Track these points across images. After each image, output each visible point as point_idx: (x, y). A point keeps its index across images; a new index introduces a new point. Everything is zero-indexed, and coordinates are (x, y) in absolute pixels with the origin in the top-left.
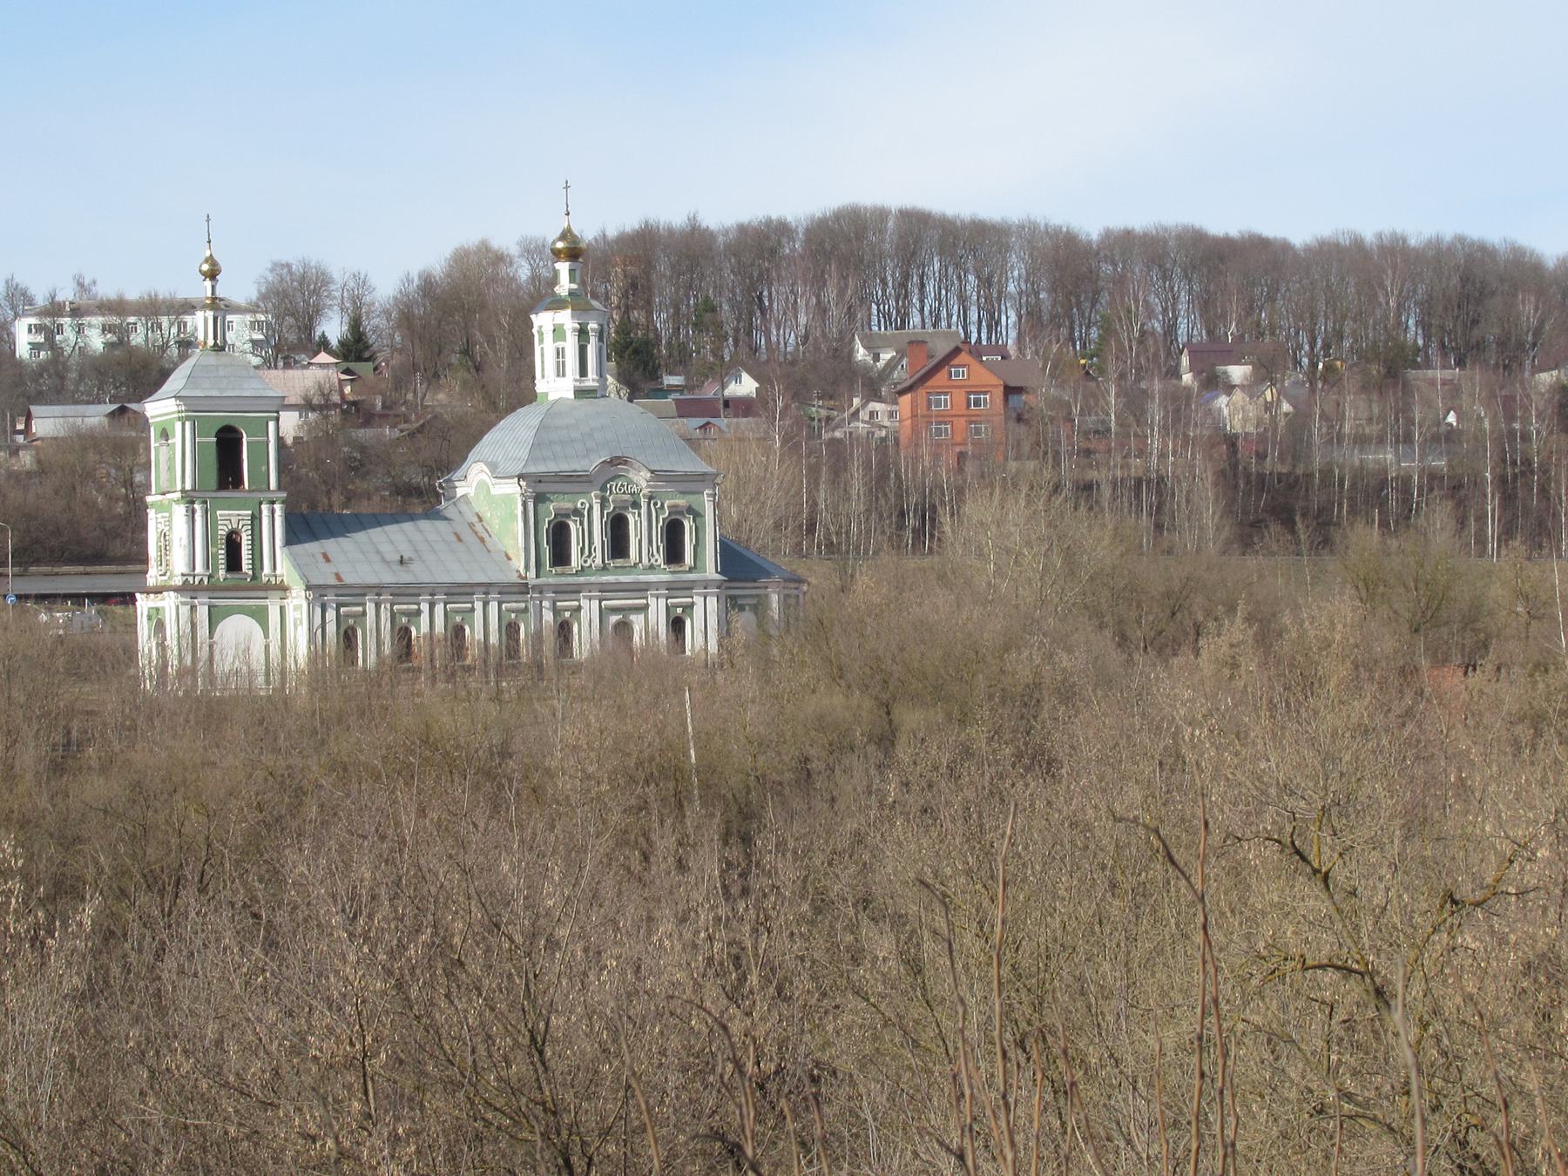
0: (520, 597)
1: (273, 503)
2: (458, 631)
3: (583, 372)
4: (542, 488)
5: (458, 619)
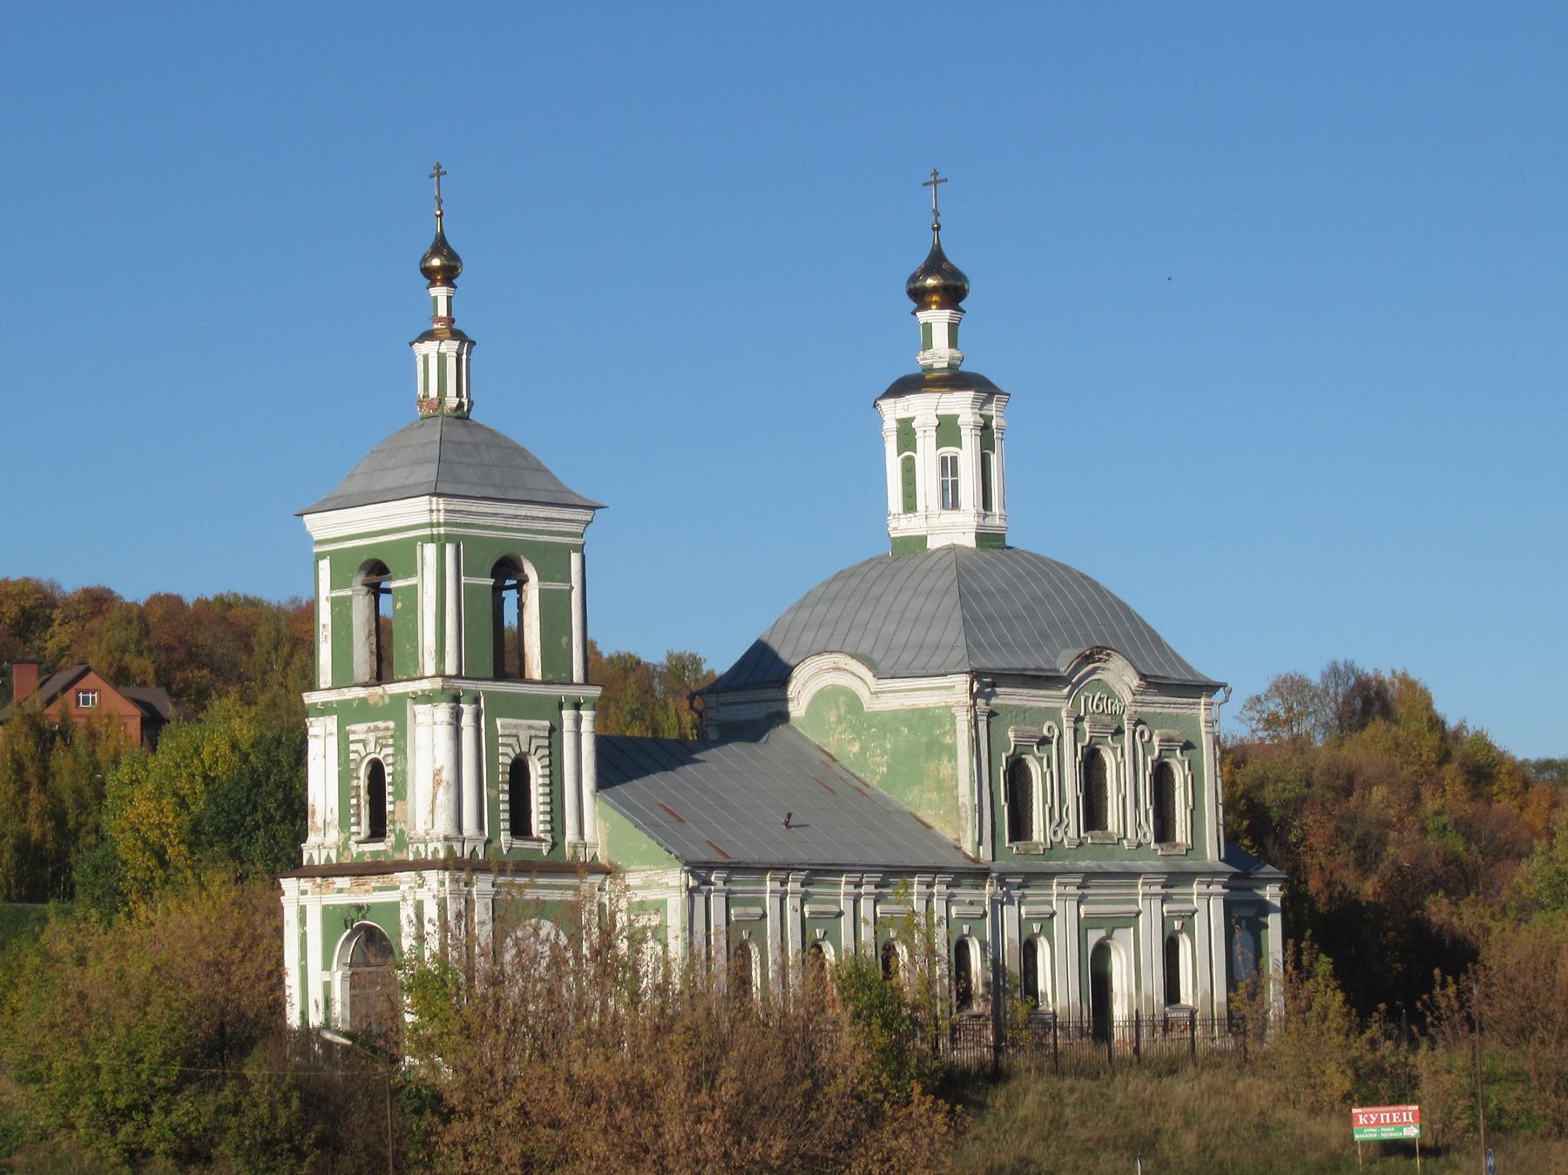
1: (577, 706)
3: (986, 503)
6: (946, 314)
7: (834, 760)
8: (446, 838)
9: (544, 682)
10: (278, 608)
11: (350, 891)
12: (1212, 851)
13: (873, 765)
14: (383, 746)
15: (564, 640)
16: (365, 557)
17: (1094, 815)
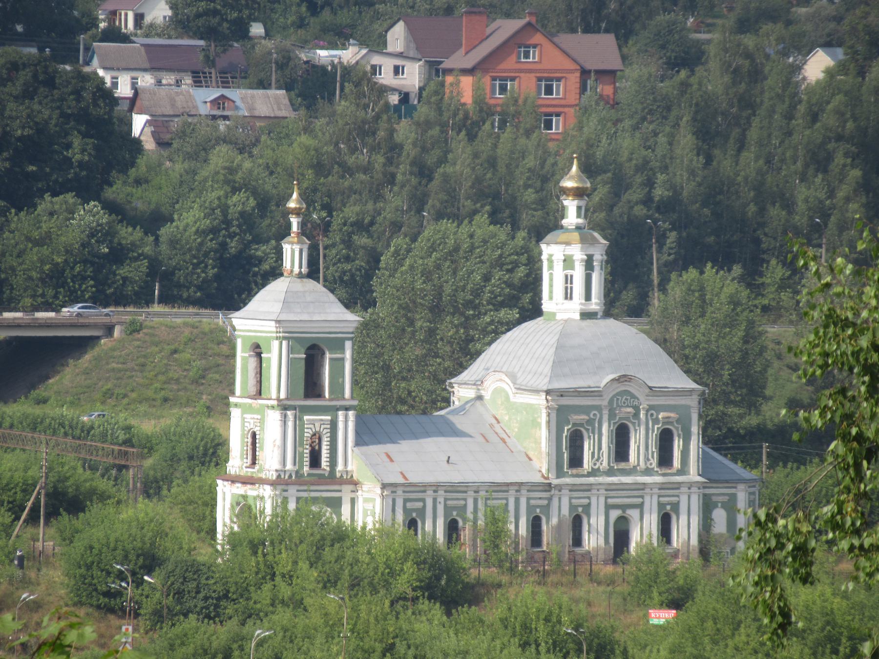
3: (588, 297)
4: (565, 401)
7: (499, 422)
8: (277, 471)
9: (330, 400)
15: (341, 380)
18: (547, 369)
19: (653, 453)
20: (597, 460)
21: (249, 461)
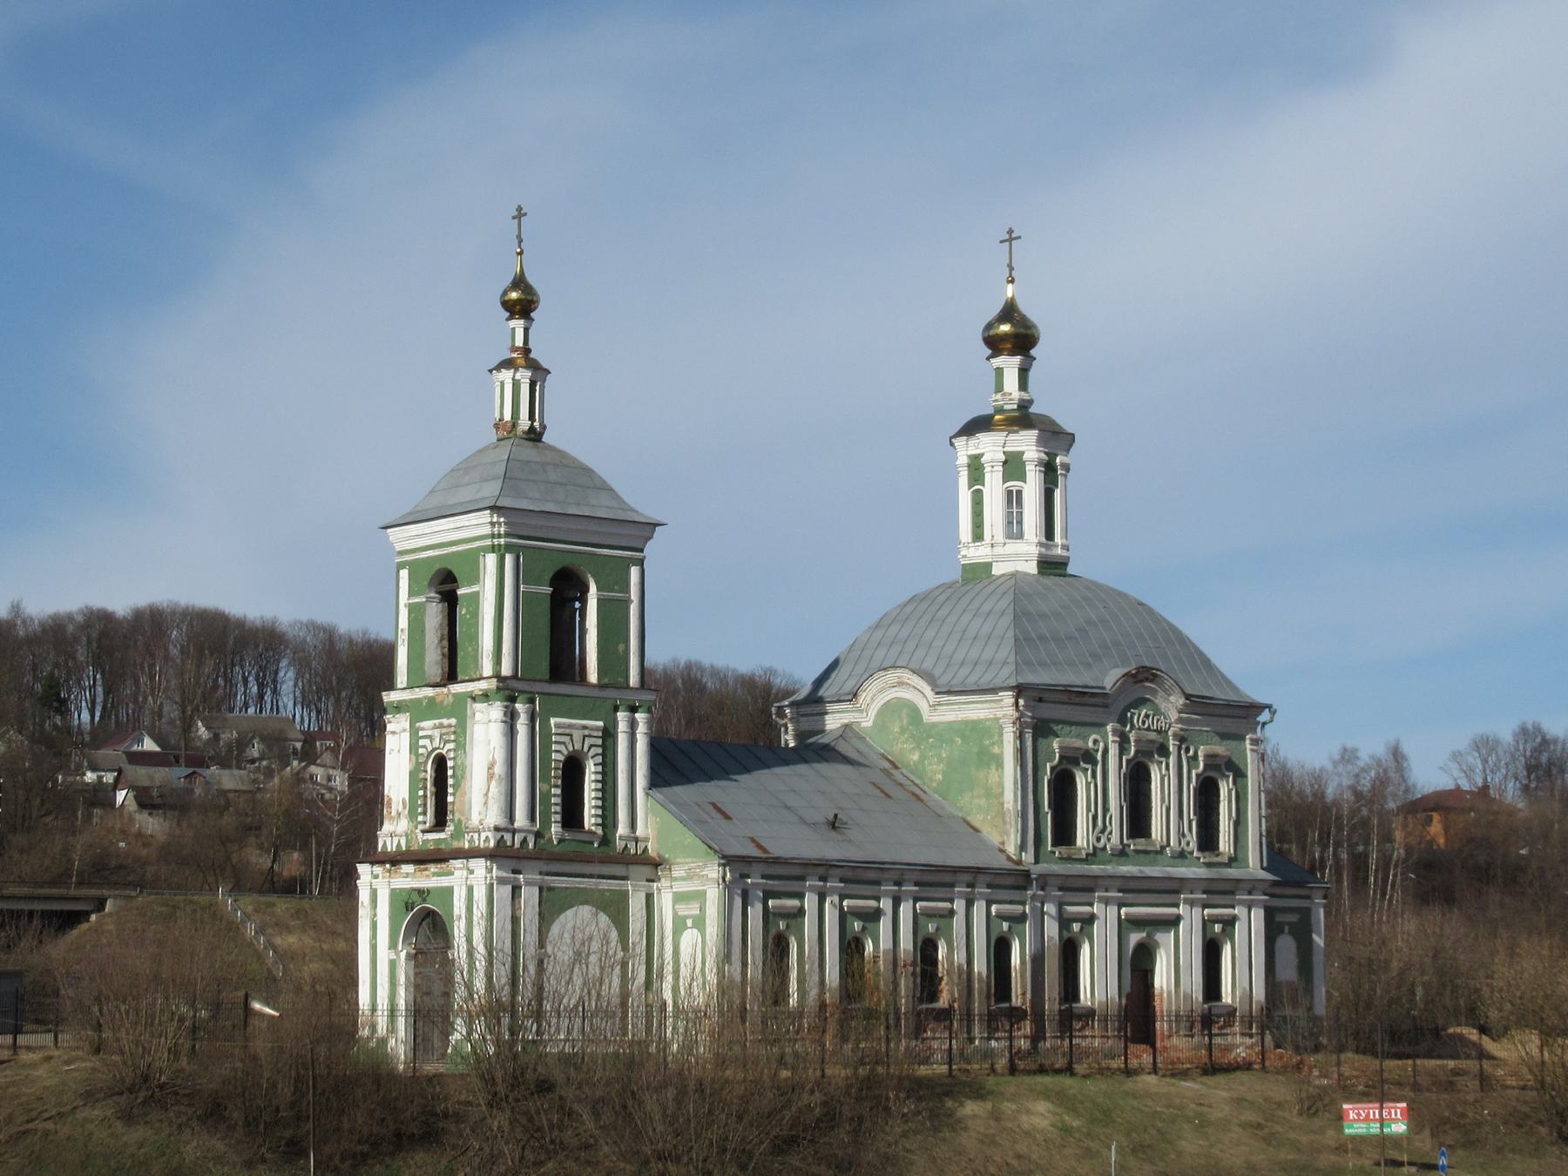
0: (1015, 895)
1: (633, 709)
2: (926, 949)
4: (1047, 711)
5: (931, 928)
6: (1017, 360)
7: (896, 767)
8: (497, 829)
10: (665, 670)
11: (413, 875)
12: (1253, 864)
13: (931, 768)
14: (447, 742)
15: (621, 647)
16: (437, 566)
17: (1138, 821)
18: (1006, 651)
19: (1190, 822)
20: (1103, 831)
21: (430, 817)
